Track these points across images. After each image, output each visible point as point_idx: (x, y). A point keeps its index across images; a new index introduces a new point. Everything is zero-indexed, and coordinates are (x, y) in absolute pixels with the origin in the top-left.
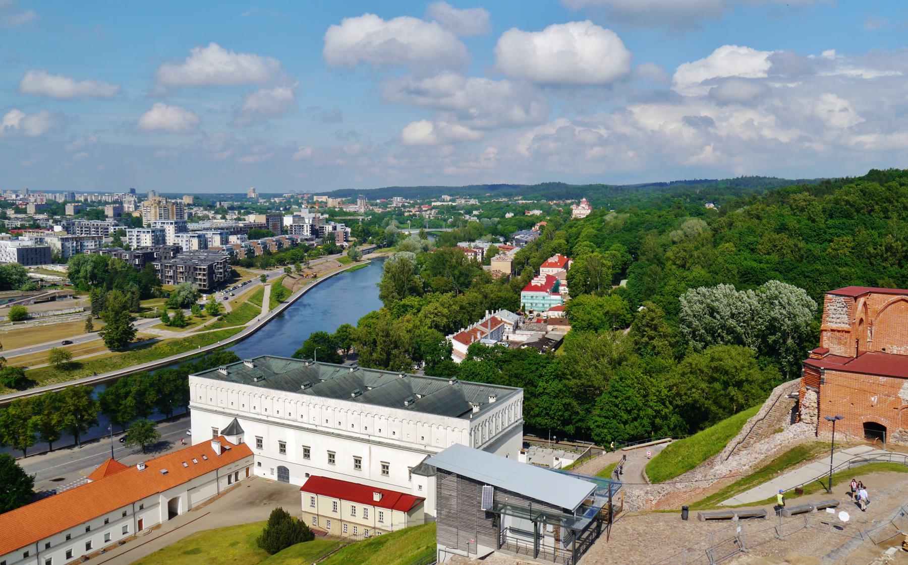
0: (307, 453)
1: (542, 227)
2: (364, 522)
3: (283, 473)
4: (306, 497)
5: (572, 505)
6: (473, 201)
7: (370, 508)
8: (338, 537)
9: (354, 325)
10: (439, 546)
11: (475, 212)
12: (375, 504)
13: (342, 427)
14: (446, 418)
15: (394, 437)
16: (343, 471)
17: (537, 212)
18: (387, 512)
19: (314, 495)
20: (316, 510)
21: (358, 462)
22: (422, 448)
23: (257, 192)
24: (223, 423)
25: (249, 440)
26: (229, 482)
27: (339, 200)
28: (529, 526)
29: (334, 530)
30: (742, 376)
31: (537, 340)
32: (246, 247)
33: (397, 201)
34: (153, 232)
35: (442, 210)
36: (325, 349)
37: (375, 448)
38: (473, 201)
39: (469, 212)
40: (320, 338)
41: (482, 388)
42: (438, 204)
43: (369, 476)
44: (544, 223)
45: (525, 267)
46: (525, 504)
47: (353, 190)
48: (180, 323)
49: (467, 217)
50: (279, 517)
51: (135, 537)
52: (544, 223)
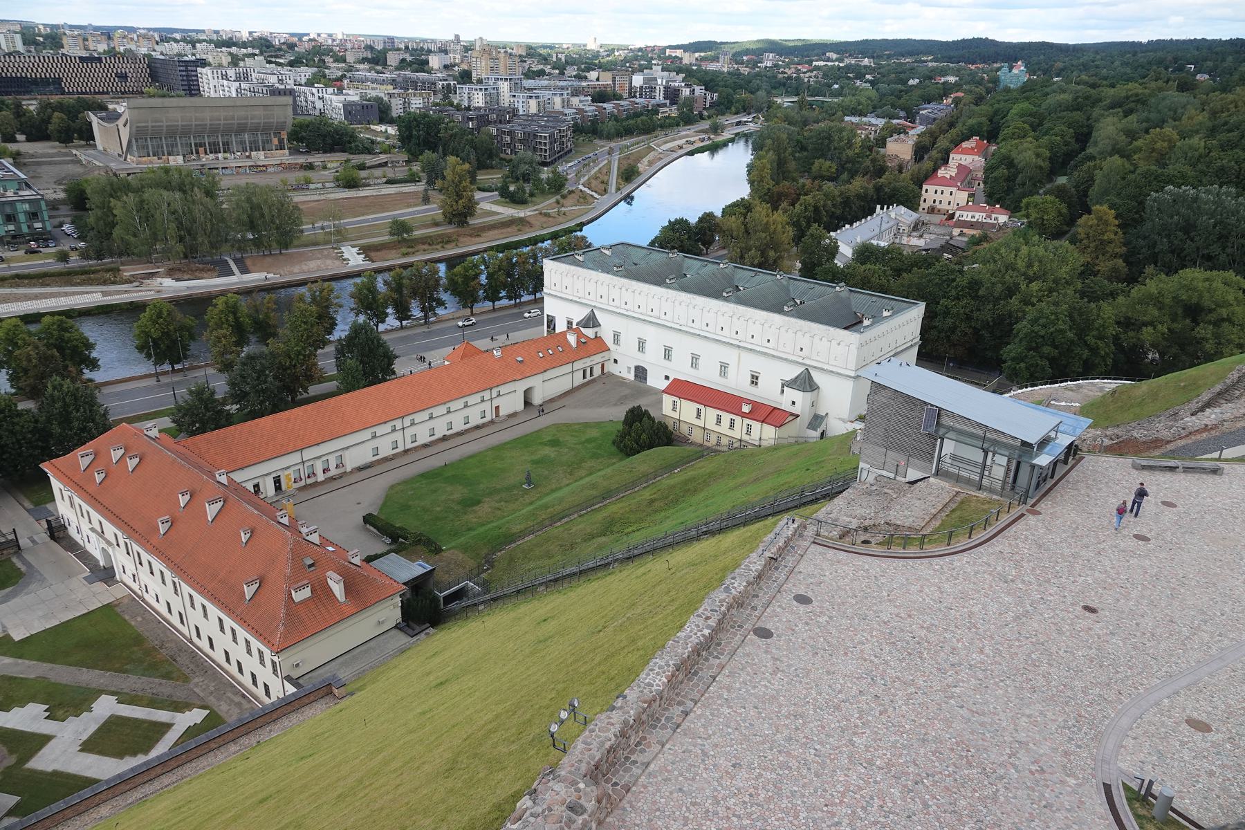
0: (667, 353)
1: (957, 101)
2: (730, 433)
3: (641, 373)
4: (668, 400)
5: (1033, 439)
6: (866, 61)
7: (738, 419)
8: (701, 445)
9: (718, 213)
10: (862, 465)
11: (868, 77)
12: (743, 415)
14: (832, 329)
16: (707, 376)
17: (952, 79)
18: (756, 426)
19: (676, 399)
20: (682, 413)
21: (724, 367)
22: (800, 360)
23: (599, 43)
24: (578, 315)
25: (607, 335)
26: (584, 377)
27: (697, 55)
28: (978, 456)
29: (697, 437)
30: (1224, 312)
31: (938, 246)
35: (827, 72)
37: (744, 355)
38: (866, 61)
39: (860, 76)
41: (874, 299)
42: (822, 63)
43: (736, 383)
44: (960, 94)
45: (931, 154)
46: (980, 432)
47: (715, 42)
48: (516, 200)
49: (858, 83)
50: (636, 416)
51: (492, 422)
52: (960, 94)
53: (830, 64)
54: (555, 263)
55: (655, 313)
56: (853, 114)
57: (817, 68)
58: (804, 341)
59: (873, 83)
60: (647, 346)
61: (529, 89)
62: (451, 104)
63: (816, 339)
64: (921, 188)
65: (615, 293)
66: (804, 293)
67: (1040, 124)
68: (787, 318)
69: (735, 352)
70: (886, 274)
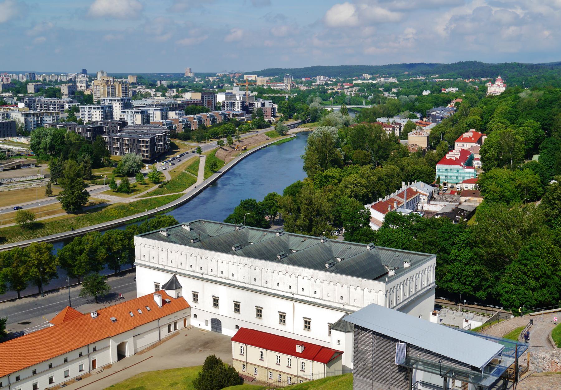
1: (457, 104)
3: (216, 324)
4: (236, 346)
6: (392, 80)
7: (293, 359)
8: (265, 383)
9: (280, 193)
11: (394, 90)
12: (297, 355)
13: (269, 285)
14: (363, 280)
15: (315, 296)
16: (269, 325)
17: (453, 90)
19: (243, 345)
20: (247, 359)
22: (341, 306)
24: (164, 279)
25: (187, 296)
26: (169, 331)
27: (267, 78)
32: (183, 121)
33: (321, 79)
34: (102, 108)
36: (255, 214)
37: (298, 305)
38: (392, 80)
39: (388, 90)
40: (248, 205)
41: (397, 254)
42: (359, 82)
43: (293, 330)
44: (459, 100)
45: (441, 142)
47: (281, 69)
48: (127, 190)
49: (386, 94)
51: (89, 374)
53: (364, 81)
54: (141, 238)
55: (225, 275)
56: (383, 116)
57: (357, 85)
58: (343, 291)
59: (397, 94)
60: (220, 302)
61: (137, 107)
62: (75, 120)
63: (352, 288)
64: (435, 168)
65: (192, 261)
66: (343, 253)
67: (516, 119)
68: (328, 274)
69: (290, 303)
70: (417, 235)
